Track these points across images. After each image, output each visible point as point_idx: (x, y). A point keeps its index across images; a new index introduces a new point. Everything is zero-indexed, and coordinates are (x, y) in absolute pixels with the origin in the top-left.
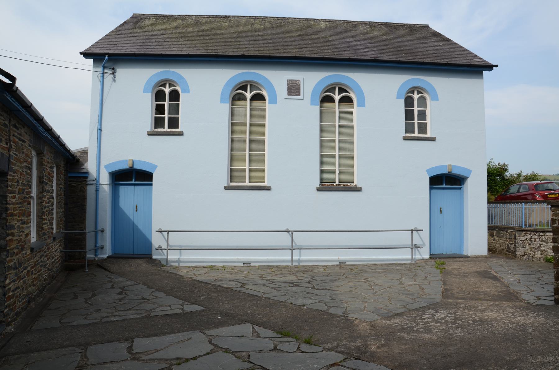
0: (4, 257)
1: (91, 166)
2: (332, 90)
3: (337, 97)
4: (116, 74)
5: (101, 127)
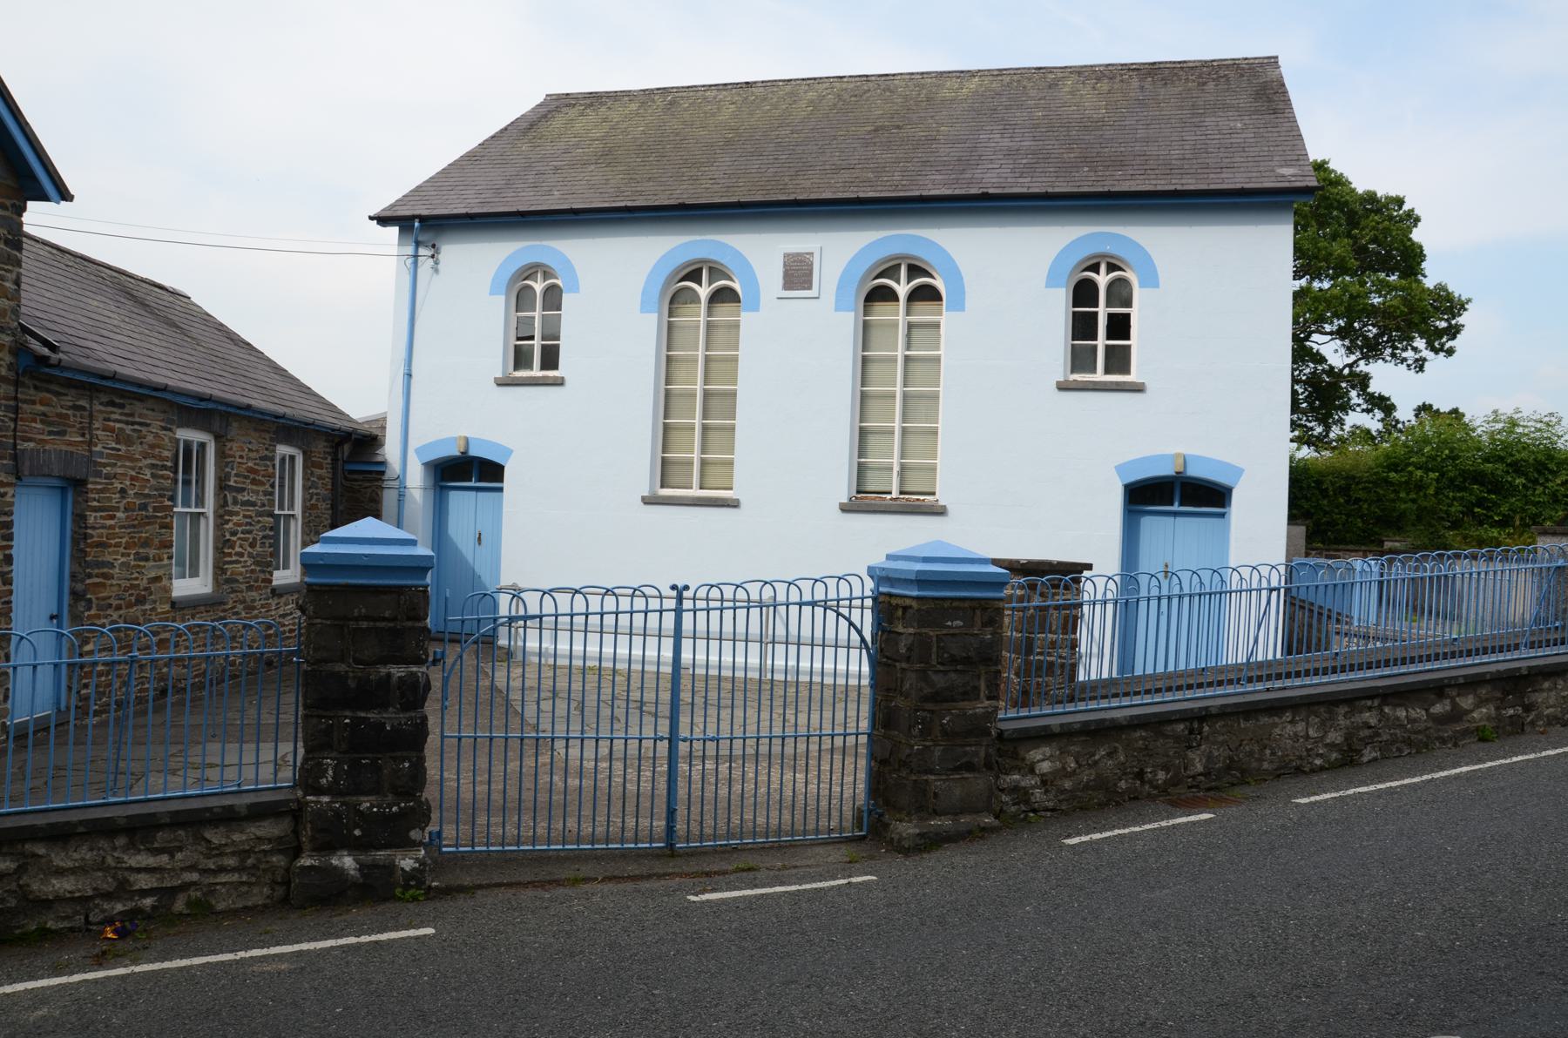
0: (82, 609)
1: (391, 450)
2: (891, 271)
3: (902, 289)
4: (441, 257)
5: (410, 370)
